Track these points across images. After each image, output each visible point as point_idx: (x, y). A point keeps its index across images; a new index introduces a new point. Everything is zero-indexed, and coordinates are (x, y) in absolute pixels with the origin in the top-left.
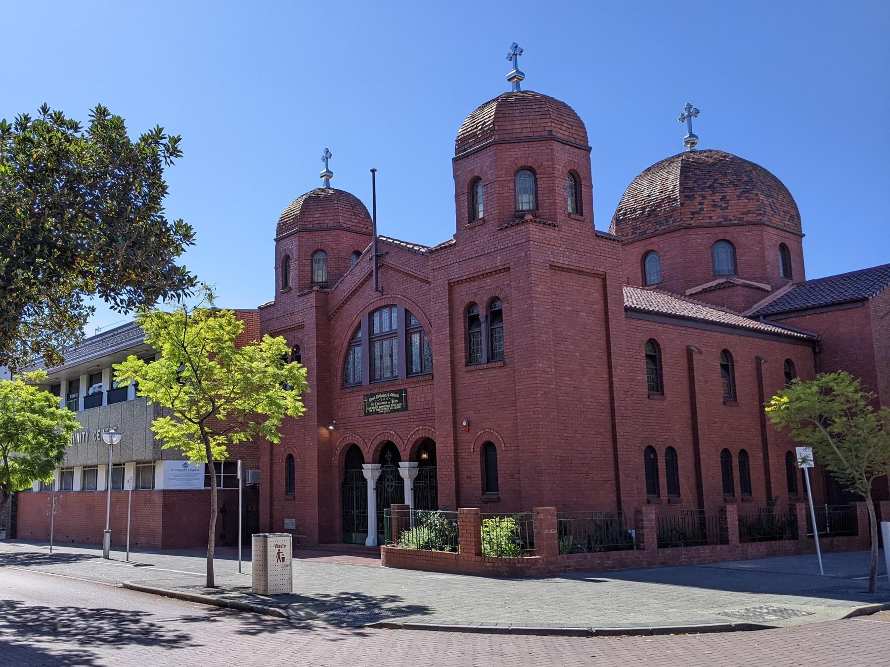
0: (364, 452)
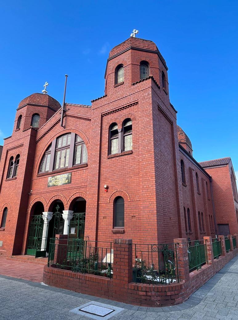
0: (45, 206)
